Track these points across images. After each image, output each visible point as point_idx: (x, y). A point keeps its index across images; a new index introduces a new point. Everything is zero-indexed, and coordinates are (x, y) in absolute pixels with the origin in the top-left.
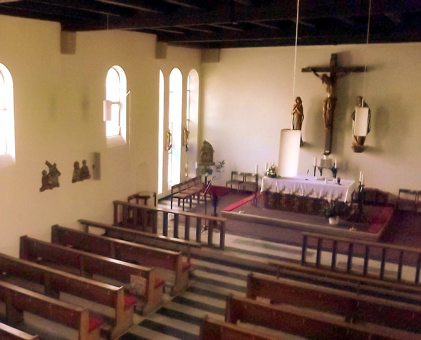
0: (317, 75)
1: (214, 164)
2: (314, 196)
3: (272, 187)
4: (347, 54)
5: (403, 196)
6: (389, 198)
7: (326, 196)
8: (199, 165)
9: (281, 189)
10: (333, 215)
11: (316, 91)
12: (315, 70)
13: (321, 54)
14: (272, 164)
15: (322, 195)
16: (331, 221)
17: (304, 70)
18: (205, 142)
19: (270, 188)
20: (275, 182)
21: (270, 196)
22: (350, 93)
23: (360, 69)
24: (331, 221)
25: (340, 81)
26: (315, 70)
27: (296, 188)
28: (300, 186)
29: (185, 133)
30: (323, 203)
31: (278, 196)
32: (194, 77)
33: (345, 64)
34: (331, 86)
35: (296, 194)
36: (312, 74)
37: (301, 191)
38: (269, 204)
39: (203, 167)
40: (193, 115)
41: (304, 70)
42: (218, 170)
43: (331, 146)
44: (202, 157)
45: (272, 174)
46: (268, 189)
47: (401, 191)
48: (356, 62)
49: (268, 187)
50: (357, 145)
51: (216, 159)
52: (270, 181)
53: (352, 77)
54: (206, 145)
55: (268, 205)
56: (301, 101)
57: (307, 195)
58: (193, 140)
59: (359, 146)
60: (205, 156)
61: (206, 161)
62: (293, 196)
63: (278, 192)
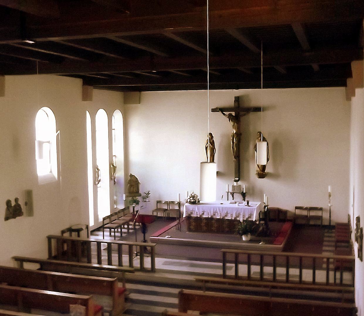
0: (224, 114)
1: (140, 195)
2: (228, 218)
3: (193, 212)
4: (247, 96)
5: (298, 212)
6: (288, 215)
7: (238, 217)
8: (127, 197)
9: (201, 214)
10: (245, 233)
11: (223, 127)
12: (222, 110)
13: (227, 96)
14: (192, 193)
15: (235, 217)
16: (244, 238)
17: (214, 110)
18: (131, 176)
19: (192, 213)
20: (195, 207)
21: (191, 220)
22: (251, 128)
23: (258, 109)
24: (244, 238)
25: (242, 119)
26: (222, 110)
27: (214, 212)
28: (216, 210)
29: (113, 168)
30: (236, 223)
31: (199, 219)
32: (118, 116)
33: (246, 105)
34: (236, 124)
35: (214, 217)
36: (220, 113)
37: (218, 214)
38: (192, 227)
39: (130, 198)
40: (119, 160)
41: (214, 110)
42: (145, 200)
43: (239, 173)
44: (129, 189)
45: (192, 201)
46: (190, 215)
47: (297, 208)
48: (254, 103)
49: (189, 213)
50: (260, 172)
51: (142, 190)
52: (191, 207)
53: (252, 116)
54: (133, 178)
55: (191, 228)
56: (212, 137)
57: (223, 217)
58: (120, 174)
59: (262, 172)
60: (132, 188)
61: (133, 192)
62: (212, 218)
63: (199, 216)
